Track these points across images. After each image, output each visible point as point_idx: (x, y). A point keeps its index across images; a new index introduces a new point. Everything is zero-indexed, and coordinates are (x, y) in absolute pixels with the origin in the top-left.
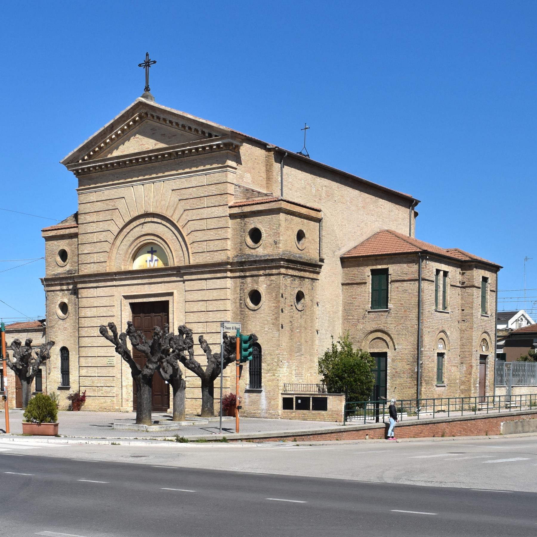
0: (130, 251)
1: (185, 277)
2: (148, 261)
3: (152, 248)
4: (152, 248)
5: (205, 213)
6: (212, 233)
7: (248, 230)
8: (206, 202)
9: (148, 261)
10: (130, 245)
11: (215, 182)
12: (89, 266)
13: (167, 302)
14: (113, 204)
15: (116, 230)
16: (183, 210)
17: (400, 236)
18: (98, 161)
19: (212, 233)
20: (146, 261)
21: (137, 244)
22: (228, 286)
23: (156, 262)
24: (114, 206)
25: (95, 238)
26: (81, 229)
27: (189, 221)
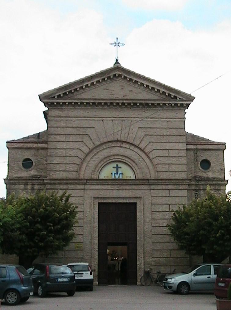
0: (100, 165)
1: (152, 187)
2: (113, 174)
3: (117, 165)
4: (117, 165)
5: (168, 146)
6: (174, 160)
7: (201, 160)
8: (72, 138)
9: (113, 174)
10: (100, 162)
11: (176, 127)
12: (58, 173)
13: (135, 204)
14: (84, 130)
15: (86, 150)
16: (149, 142)
17: (128, 165)
18: (76, 99)
19: (174, 160)
20: (112, 174)
21: (127, 161)
22: (86, 188)
23: (121, 175)
24: (85, 132)
25: (60, 152)
26: (51, 145)
27: (153, 150)
